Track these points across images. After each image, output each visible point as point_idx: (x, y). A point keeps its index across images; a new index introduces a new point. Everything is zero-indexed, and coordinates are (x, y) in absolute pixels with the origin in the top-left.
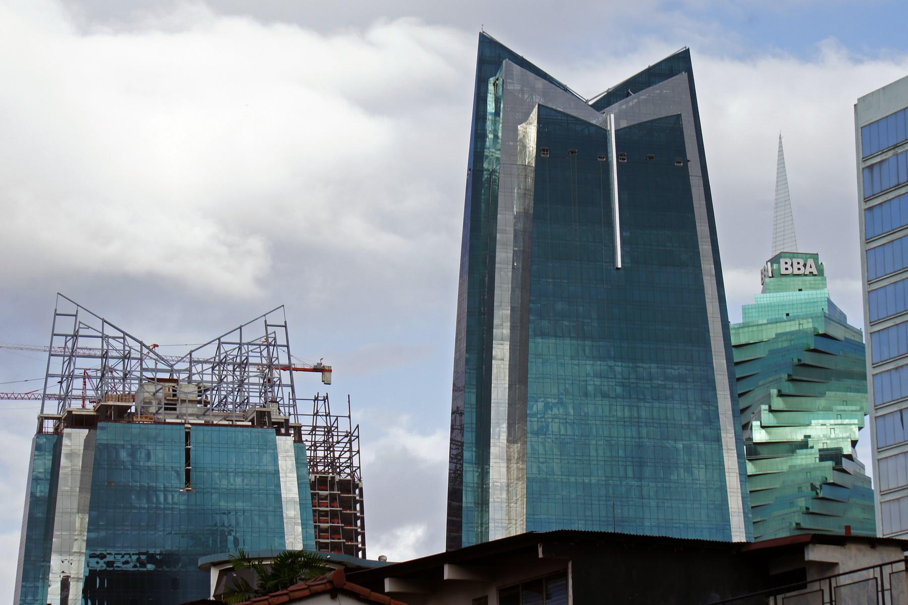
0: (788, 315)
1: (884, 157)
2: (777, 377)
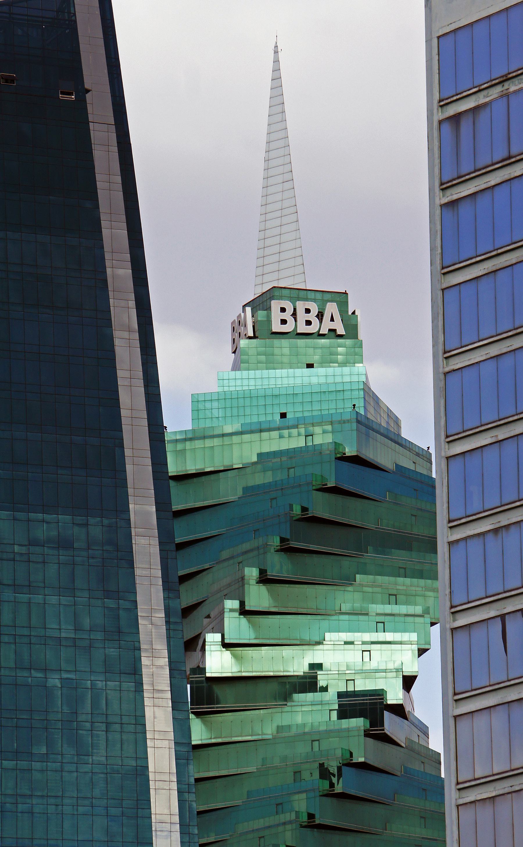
0: (283, 415)
1: (481, 99)
2: (260, 541)
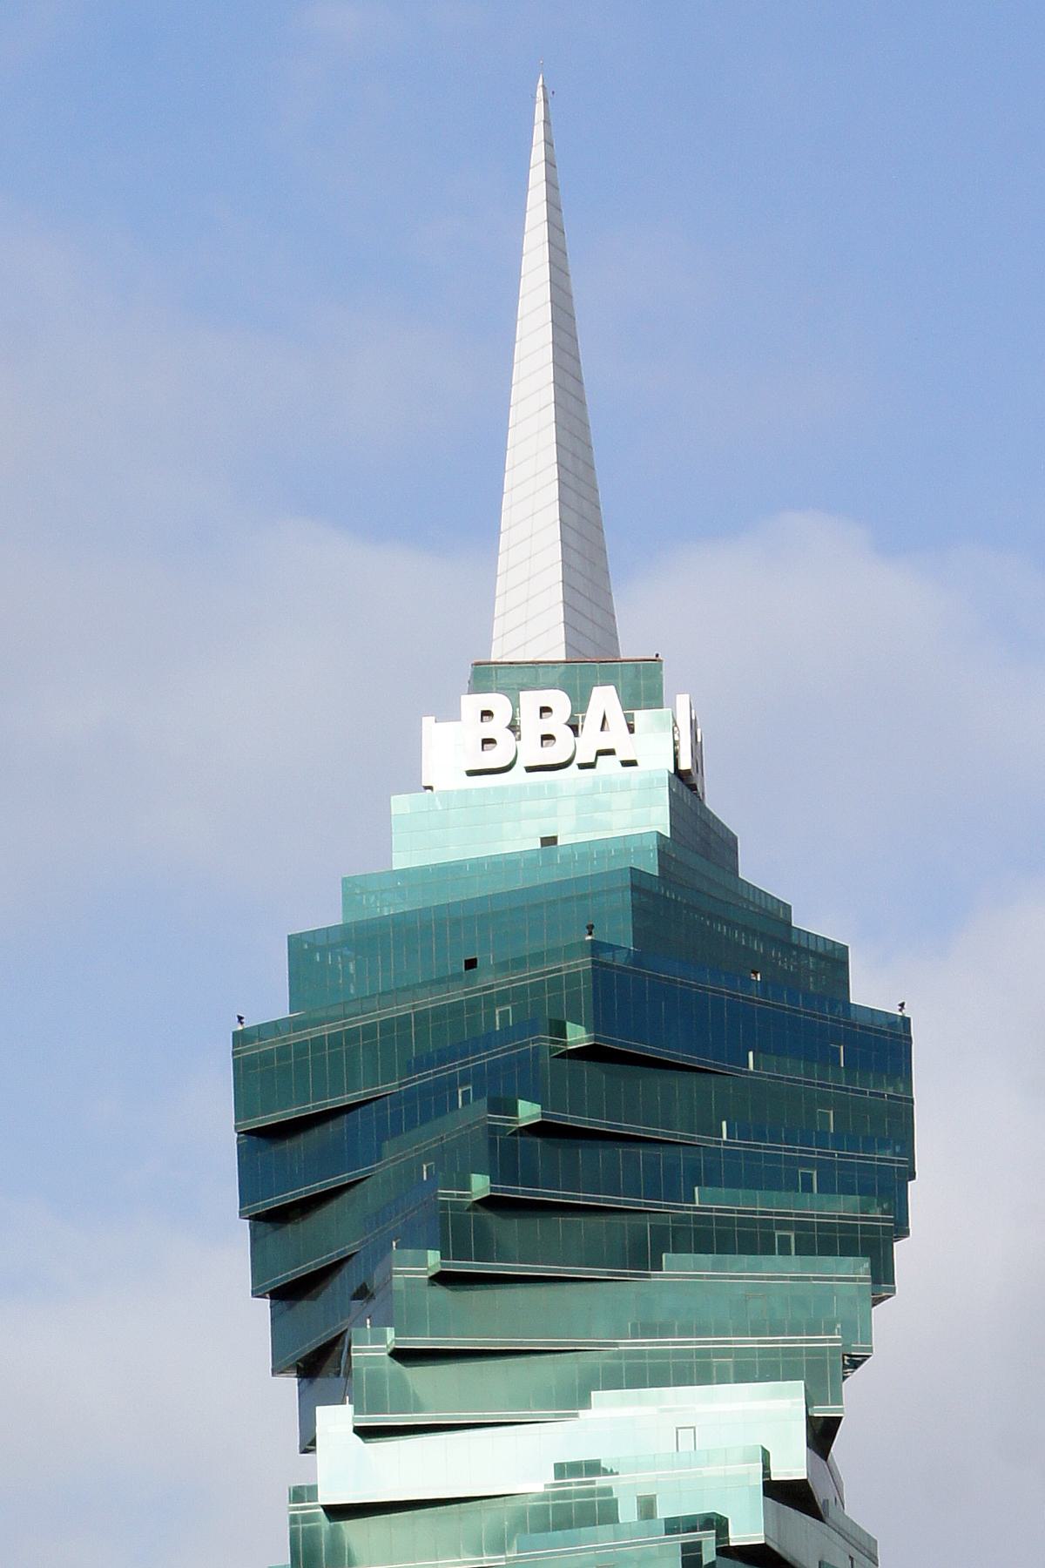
0: (549, 841)
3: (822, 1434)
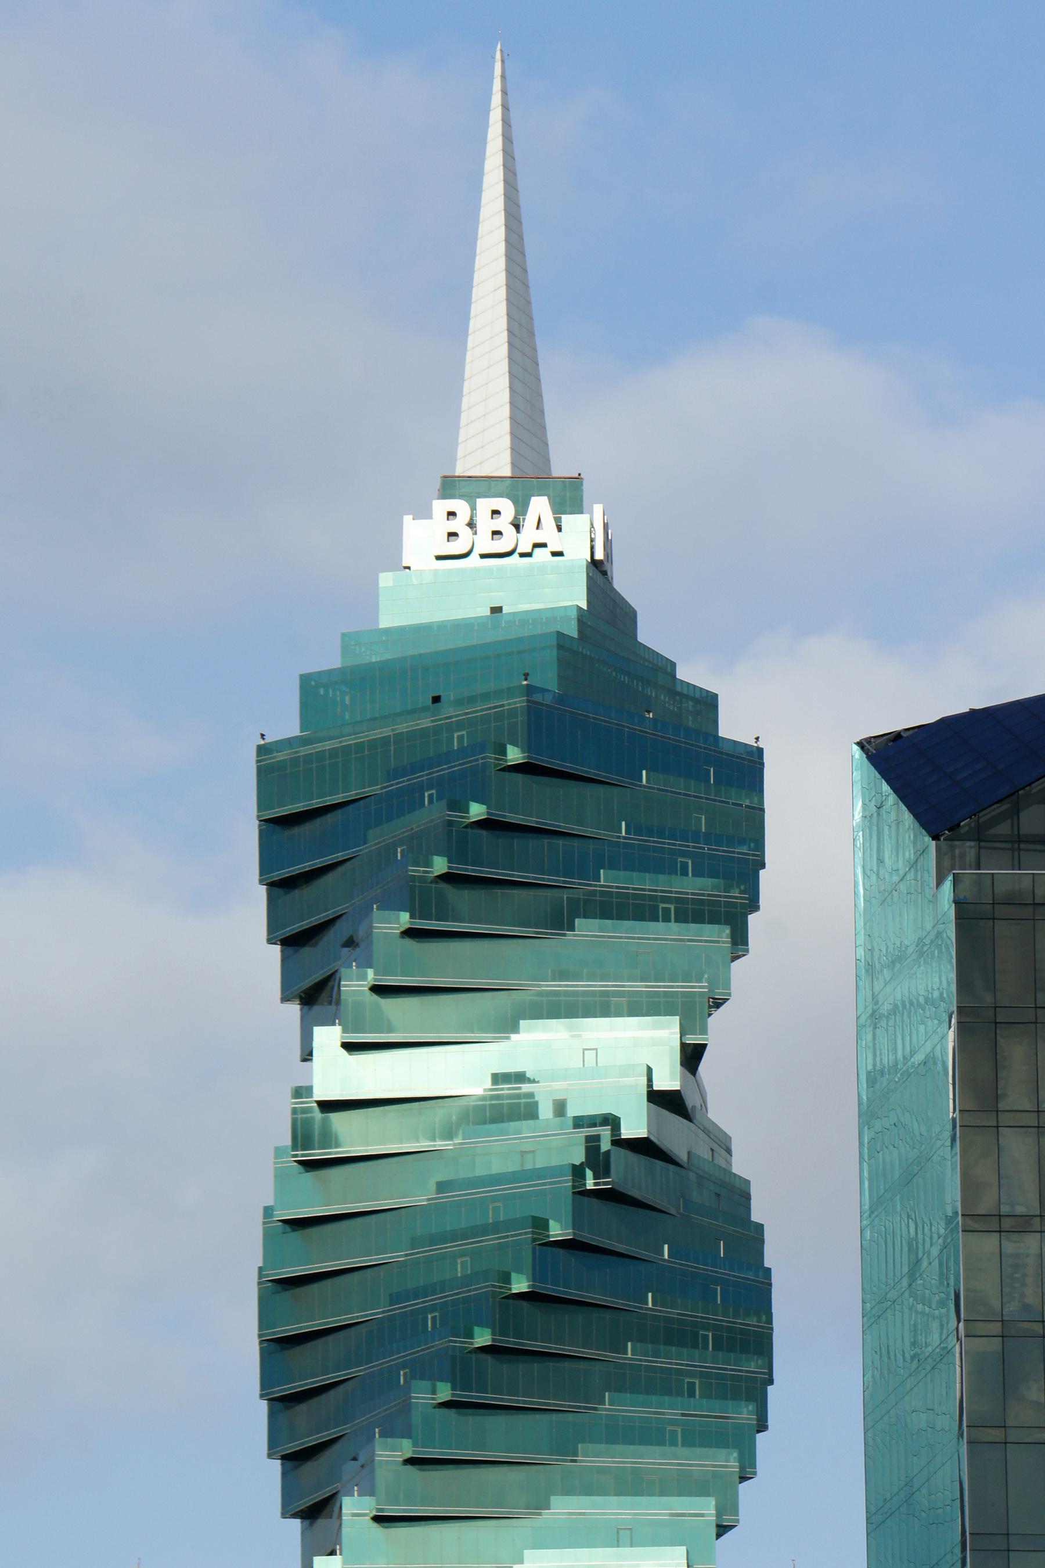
0: (496, 610)
3: (692, 1057)
